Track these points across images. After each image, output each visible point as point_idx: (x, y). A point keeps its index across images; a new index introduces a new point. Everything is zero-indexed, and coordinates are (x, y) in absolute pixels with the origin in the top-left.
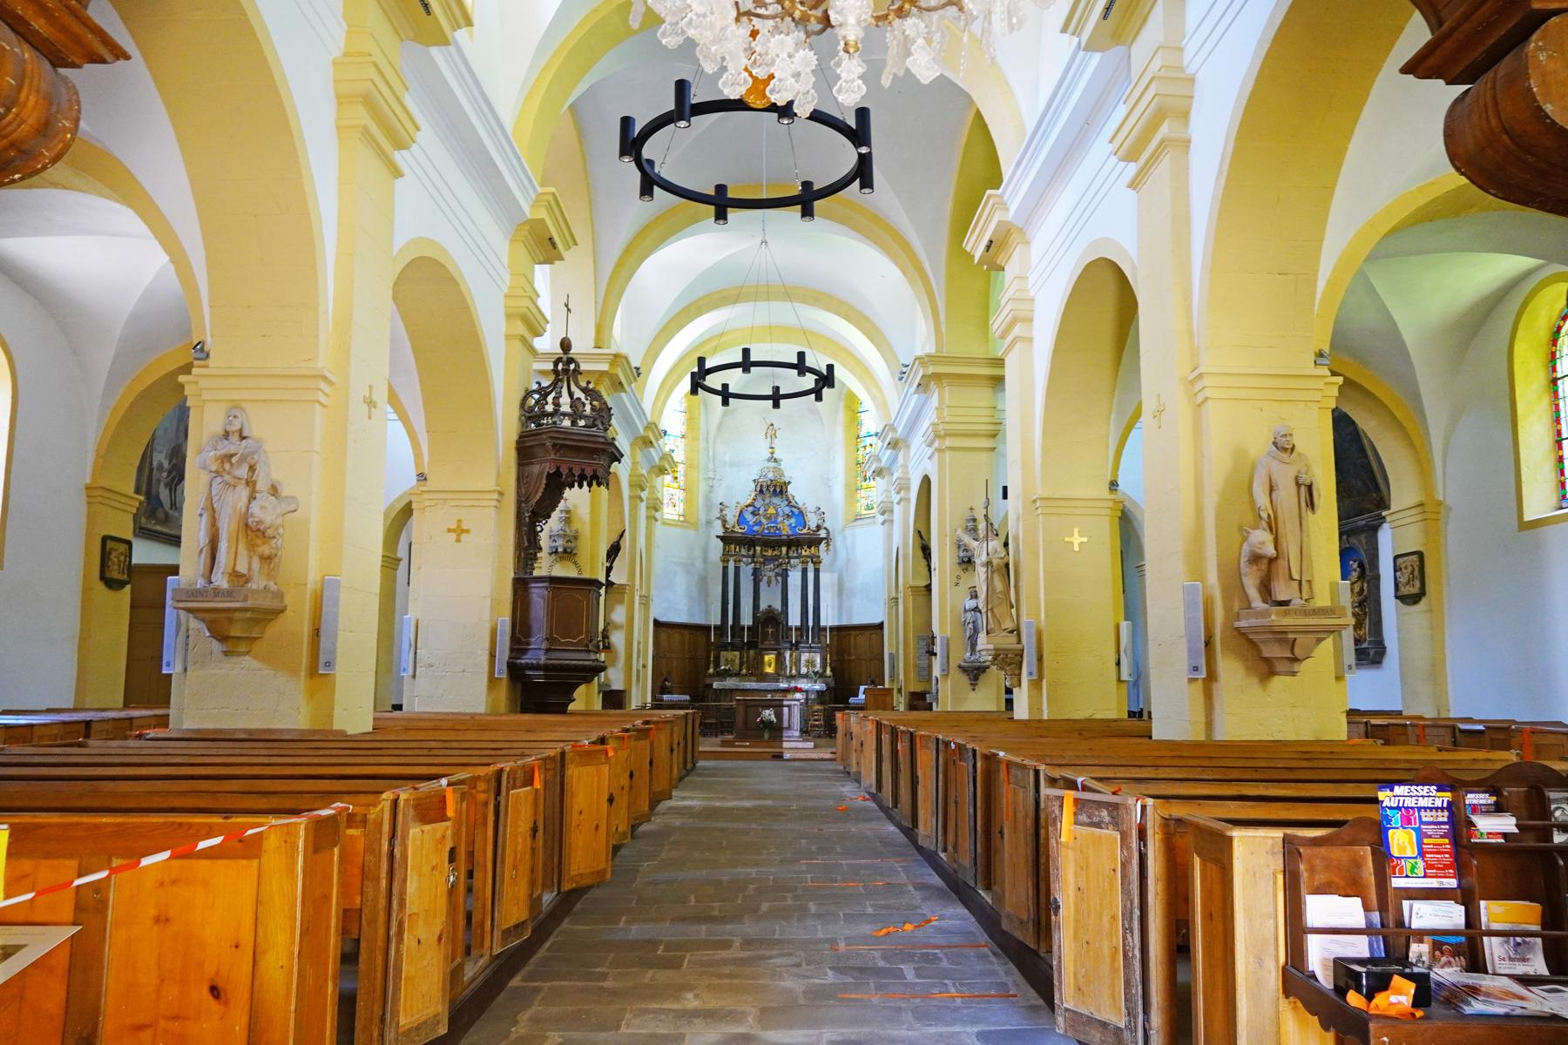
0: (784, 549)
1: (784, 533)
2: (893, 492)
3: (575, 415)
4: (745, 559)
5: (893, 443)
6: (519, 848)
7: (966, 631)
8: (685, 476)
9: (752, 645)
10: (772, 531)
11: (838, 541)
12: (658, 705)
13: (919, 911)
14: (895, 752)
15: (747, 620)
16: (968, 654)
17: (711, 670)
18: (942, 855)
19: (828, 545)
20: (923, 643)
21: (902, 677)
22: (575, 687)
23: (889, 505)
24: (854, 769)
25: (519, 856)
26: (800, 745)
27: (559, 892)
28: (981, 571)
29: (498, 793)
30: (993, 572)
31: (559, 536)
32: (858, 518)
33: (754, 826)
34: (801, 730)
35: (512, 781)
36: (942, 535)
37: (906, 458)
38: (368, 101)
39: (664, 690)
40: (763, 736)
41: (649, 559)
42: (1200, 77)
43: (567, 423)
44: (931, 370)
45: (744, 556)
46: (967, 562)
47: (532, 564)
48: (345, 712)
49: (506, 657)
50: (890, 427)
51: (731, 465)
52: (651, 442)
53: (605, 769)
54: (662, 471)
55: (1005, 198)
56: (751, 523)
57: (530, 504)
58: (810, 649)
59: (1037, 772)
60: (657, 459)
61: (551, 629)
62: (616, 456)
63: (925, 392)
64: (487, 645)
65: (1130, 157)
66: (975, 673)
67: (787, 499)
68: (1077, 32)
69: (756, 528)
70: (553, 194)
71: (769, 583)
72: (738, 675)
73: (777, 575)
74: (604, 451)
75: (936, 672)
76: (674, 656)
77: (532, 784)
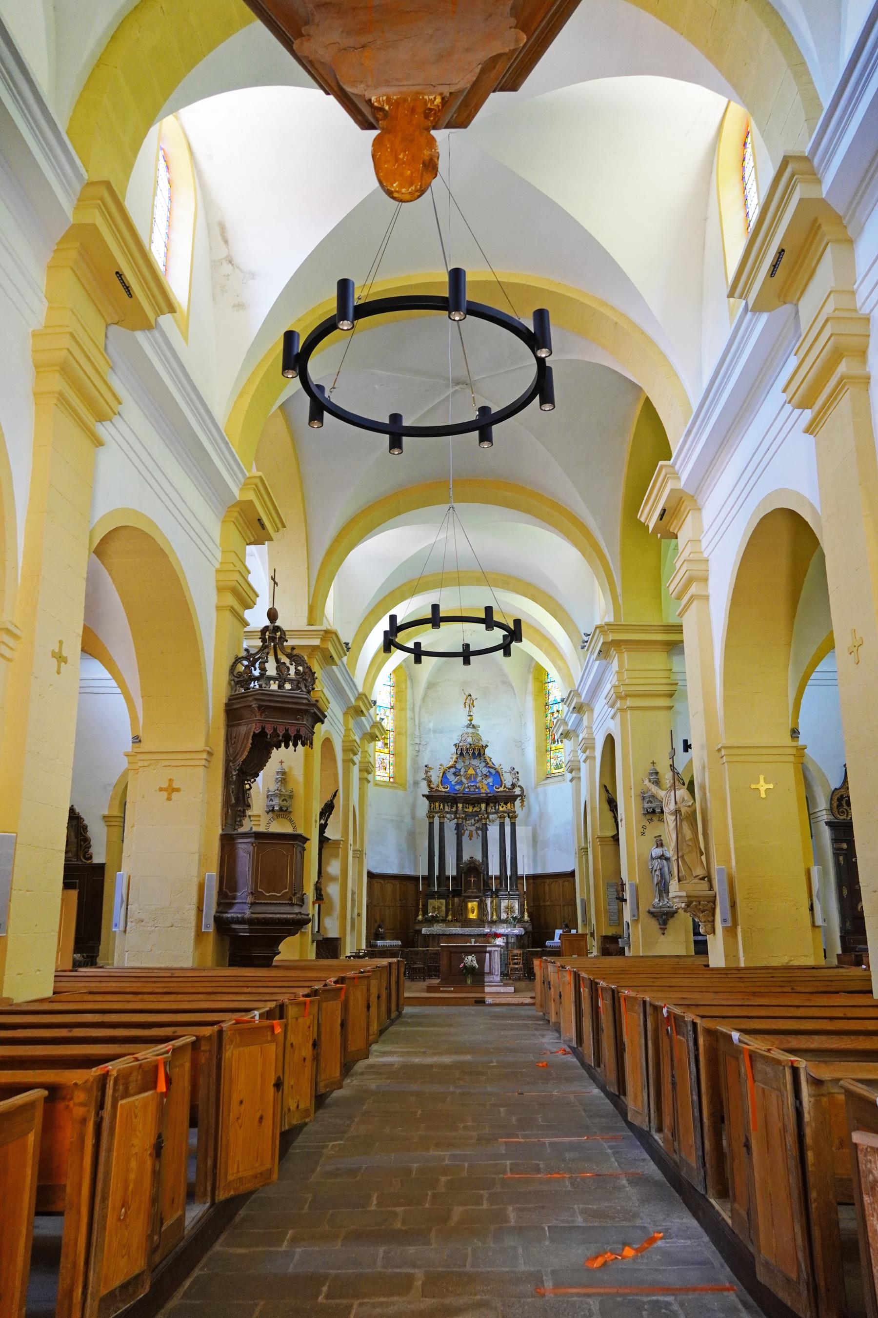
0: (483, 806)
1: (483, 791)
2: (579, 752)
3: (281, 678)
4: (448, 816)
6: (132, 1176)
7: (653, 878)
8: (395, 742)
9: (456, 893)
10: (472, 789)
11: (531, 797)
12: (373, 952)
13: (638, 1222)
14: (595, 1009)
15: (451, 870)
16: (657, 900)
17: (420, 917)
18: (657, 1137)
19: (522, 801)
20: (613, 890)
21: (594, 921)
22: (280, 940)
23: (577, 764)
24: (553, 1019)
25: (131, 1186)
26: (502, 990)
27: (213, 1203)
28: (670, 819)
29: (101, 1106)
30: (681, 821)
31: (275, 795)
32: (549, 776)
33: (452, 1089)
34: (502, 973)
35: (121, 1088)
36: (627, 788)
37: (591, 720)
38: (65, 370)
39: (378, 936)
40: (466, 981)
41: (362, 816)
42: (711, 558)
43: (274, 686)
44: (611, 637)
45: (447, 813)
46: (653, 813)
47: (240, 821)
48: (38, 973)
49: (213, 912)
50: (574, 693)
51: (435, 732)
52: (362, 711)
53: (272, 1047)
54: (373, 738)
55: (677, 467)
57: (237, 763)
58: (509, 897)
59: (795, 1071)
60: (368, 727)
61: (256, 882)
62: (320, 718)
63: (605, 658)
64: (194, 899)
65: (804, 404)
66: (664, 917)
67: (485, 761)
68: (743, 295)
69: (457, 787)
70: (261, 478)
71: (471, 836)
72: (444, 921)
73: (477, 829)
74: (307, 712)
75: (627, 917)
77: (155, 1087)
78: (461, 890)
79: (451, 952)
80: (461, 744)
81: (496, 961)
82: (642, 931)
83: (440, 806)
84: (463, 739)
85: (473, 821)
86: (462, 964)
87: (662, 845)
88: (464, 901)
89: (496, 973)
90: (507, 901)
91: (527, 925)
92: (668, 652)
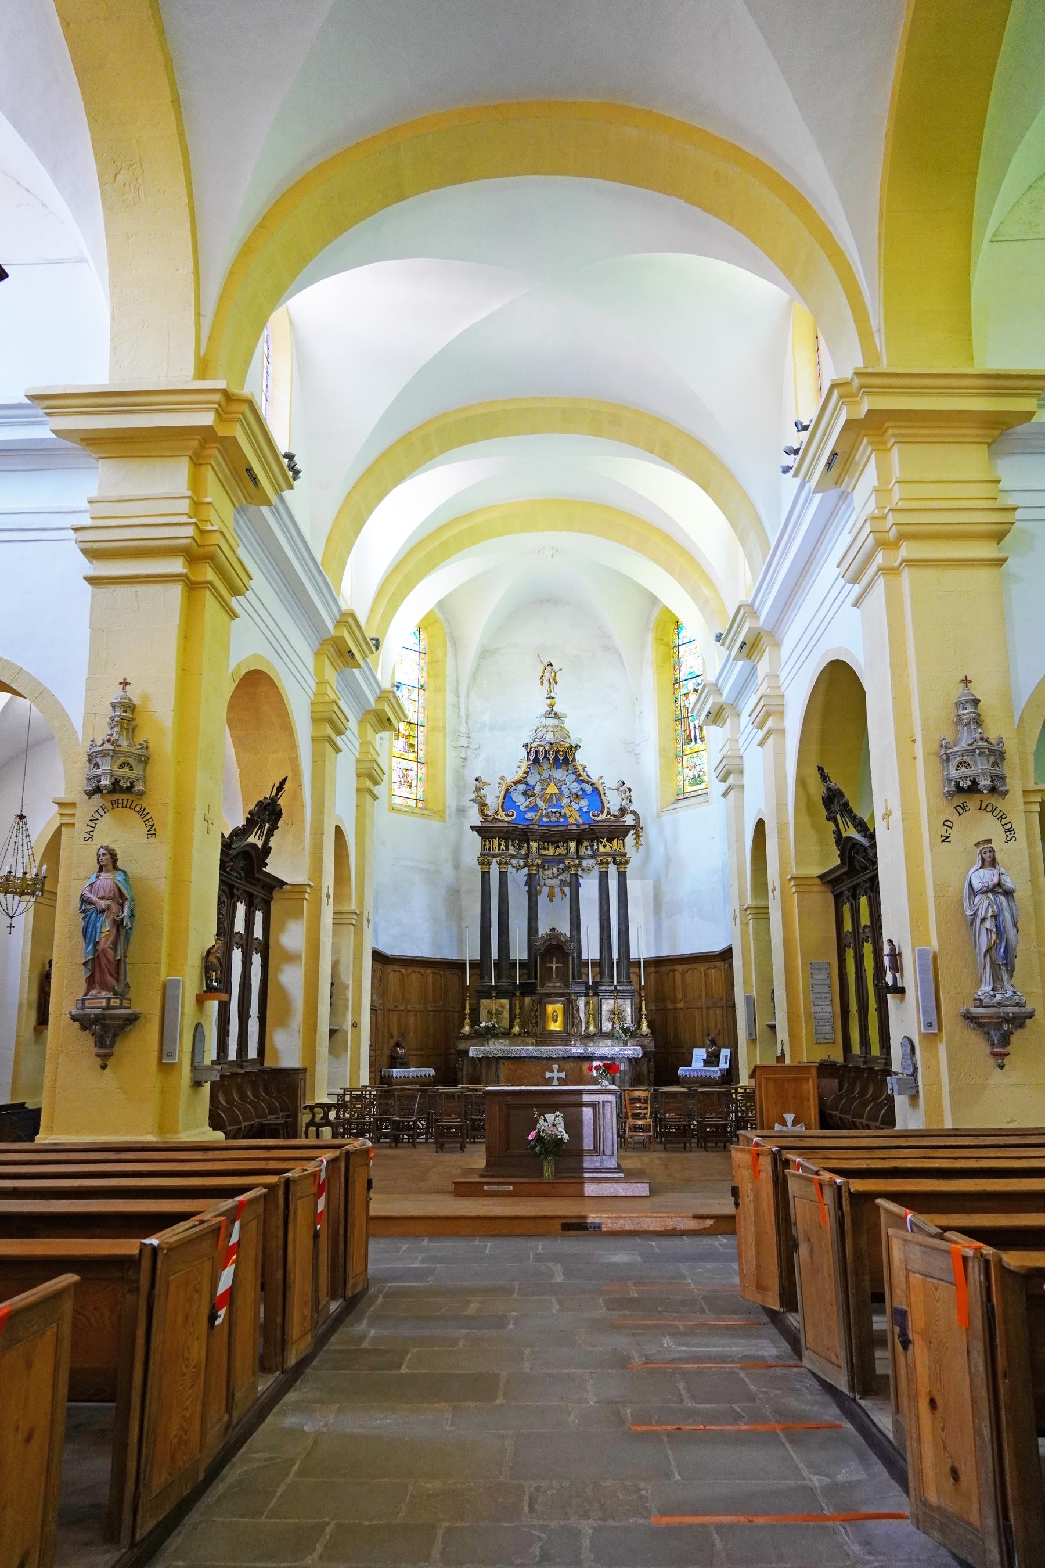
1: (571, 821)
4: (514, 862)
5: (714, 713)
7: (975, 939)
8: (426, 743)
9: (527, 989)
10: (554, 819)
11: (651, 830)
15: (519, 952)
16: (987, 988)
17: (467, 1029)
19: (638, 836)
23: (738, 761)
31: (104, 753)
39: (395, 1061)
42: (786, 694)
45: (513, 856)
58: (617, 994)
65: (854, 580)
69: (529, 815)
71: (551, 896)
72: (507, 1034)
73: (563, 883)
76: (409, 1007)
78: (535, 984)
79: (510, 1107)
80: (535, 744)
81: (608, 1126)
82: (950, 1058)
83: (500, 845)
84: (539, 736)
85: (555, 870)
86: (534, 1133)
87: (993, 863)
88: (540, 1002)
89: (608, 1151)
90: (612, 1002)
91: (647, 1041)
92: (989, 445)
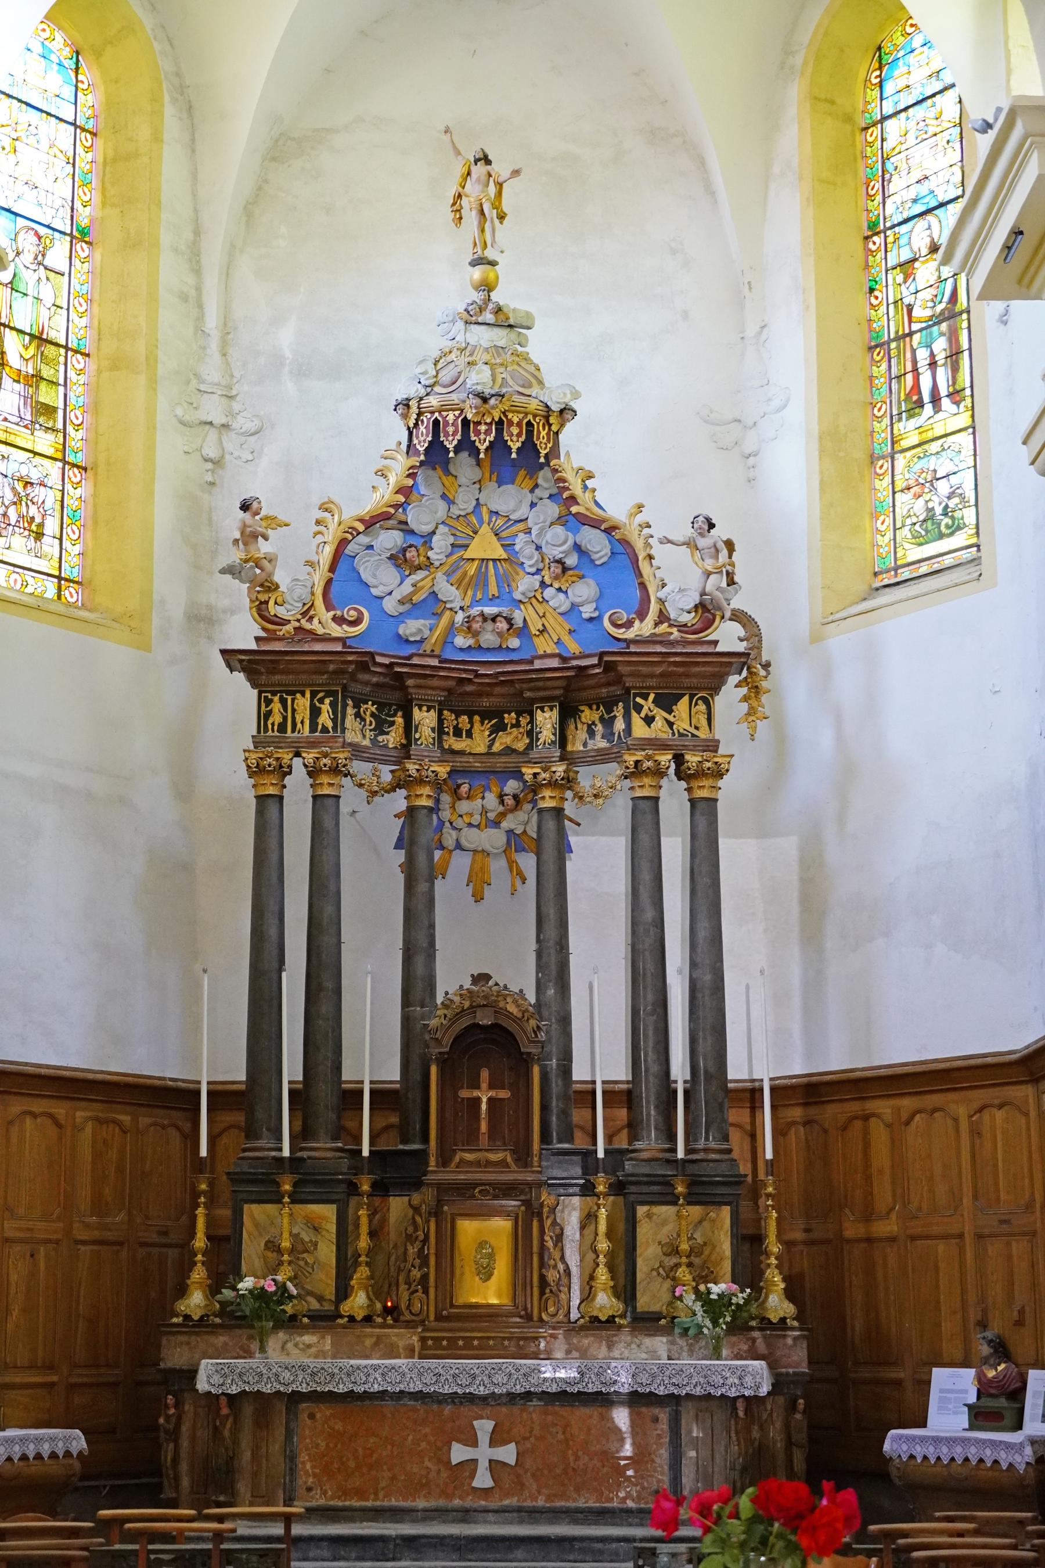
1: (544, 645)
4: (361, 768)
10: (489, 639)
17: (195, 1301)
45: (357, 752)
51: (301, 372)
56: (390, 605)
69: (411, 628)
73: (515, 842)
78: (422, 1155)
80: (433, 401)
83: (315, 712)
84: (446, 376)
85: (491, 800)
88: (436, 1213)
